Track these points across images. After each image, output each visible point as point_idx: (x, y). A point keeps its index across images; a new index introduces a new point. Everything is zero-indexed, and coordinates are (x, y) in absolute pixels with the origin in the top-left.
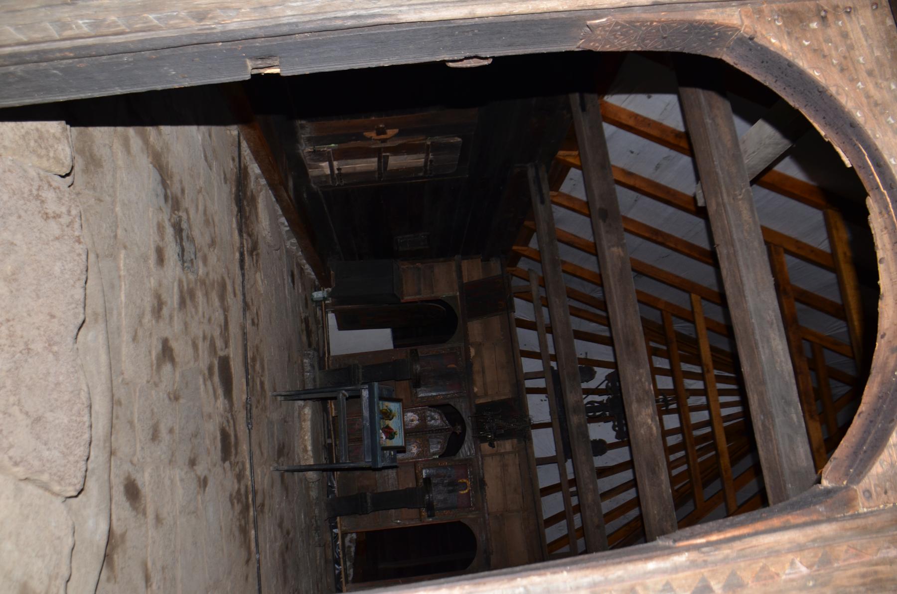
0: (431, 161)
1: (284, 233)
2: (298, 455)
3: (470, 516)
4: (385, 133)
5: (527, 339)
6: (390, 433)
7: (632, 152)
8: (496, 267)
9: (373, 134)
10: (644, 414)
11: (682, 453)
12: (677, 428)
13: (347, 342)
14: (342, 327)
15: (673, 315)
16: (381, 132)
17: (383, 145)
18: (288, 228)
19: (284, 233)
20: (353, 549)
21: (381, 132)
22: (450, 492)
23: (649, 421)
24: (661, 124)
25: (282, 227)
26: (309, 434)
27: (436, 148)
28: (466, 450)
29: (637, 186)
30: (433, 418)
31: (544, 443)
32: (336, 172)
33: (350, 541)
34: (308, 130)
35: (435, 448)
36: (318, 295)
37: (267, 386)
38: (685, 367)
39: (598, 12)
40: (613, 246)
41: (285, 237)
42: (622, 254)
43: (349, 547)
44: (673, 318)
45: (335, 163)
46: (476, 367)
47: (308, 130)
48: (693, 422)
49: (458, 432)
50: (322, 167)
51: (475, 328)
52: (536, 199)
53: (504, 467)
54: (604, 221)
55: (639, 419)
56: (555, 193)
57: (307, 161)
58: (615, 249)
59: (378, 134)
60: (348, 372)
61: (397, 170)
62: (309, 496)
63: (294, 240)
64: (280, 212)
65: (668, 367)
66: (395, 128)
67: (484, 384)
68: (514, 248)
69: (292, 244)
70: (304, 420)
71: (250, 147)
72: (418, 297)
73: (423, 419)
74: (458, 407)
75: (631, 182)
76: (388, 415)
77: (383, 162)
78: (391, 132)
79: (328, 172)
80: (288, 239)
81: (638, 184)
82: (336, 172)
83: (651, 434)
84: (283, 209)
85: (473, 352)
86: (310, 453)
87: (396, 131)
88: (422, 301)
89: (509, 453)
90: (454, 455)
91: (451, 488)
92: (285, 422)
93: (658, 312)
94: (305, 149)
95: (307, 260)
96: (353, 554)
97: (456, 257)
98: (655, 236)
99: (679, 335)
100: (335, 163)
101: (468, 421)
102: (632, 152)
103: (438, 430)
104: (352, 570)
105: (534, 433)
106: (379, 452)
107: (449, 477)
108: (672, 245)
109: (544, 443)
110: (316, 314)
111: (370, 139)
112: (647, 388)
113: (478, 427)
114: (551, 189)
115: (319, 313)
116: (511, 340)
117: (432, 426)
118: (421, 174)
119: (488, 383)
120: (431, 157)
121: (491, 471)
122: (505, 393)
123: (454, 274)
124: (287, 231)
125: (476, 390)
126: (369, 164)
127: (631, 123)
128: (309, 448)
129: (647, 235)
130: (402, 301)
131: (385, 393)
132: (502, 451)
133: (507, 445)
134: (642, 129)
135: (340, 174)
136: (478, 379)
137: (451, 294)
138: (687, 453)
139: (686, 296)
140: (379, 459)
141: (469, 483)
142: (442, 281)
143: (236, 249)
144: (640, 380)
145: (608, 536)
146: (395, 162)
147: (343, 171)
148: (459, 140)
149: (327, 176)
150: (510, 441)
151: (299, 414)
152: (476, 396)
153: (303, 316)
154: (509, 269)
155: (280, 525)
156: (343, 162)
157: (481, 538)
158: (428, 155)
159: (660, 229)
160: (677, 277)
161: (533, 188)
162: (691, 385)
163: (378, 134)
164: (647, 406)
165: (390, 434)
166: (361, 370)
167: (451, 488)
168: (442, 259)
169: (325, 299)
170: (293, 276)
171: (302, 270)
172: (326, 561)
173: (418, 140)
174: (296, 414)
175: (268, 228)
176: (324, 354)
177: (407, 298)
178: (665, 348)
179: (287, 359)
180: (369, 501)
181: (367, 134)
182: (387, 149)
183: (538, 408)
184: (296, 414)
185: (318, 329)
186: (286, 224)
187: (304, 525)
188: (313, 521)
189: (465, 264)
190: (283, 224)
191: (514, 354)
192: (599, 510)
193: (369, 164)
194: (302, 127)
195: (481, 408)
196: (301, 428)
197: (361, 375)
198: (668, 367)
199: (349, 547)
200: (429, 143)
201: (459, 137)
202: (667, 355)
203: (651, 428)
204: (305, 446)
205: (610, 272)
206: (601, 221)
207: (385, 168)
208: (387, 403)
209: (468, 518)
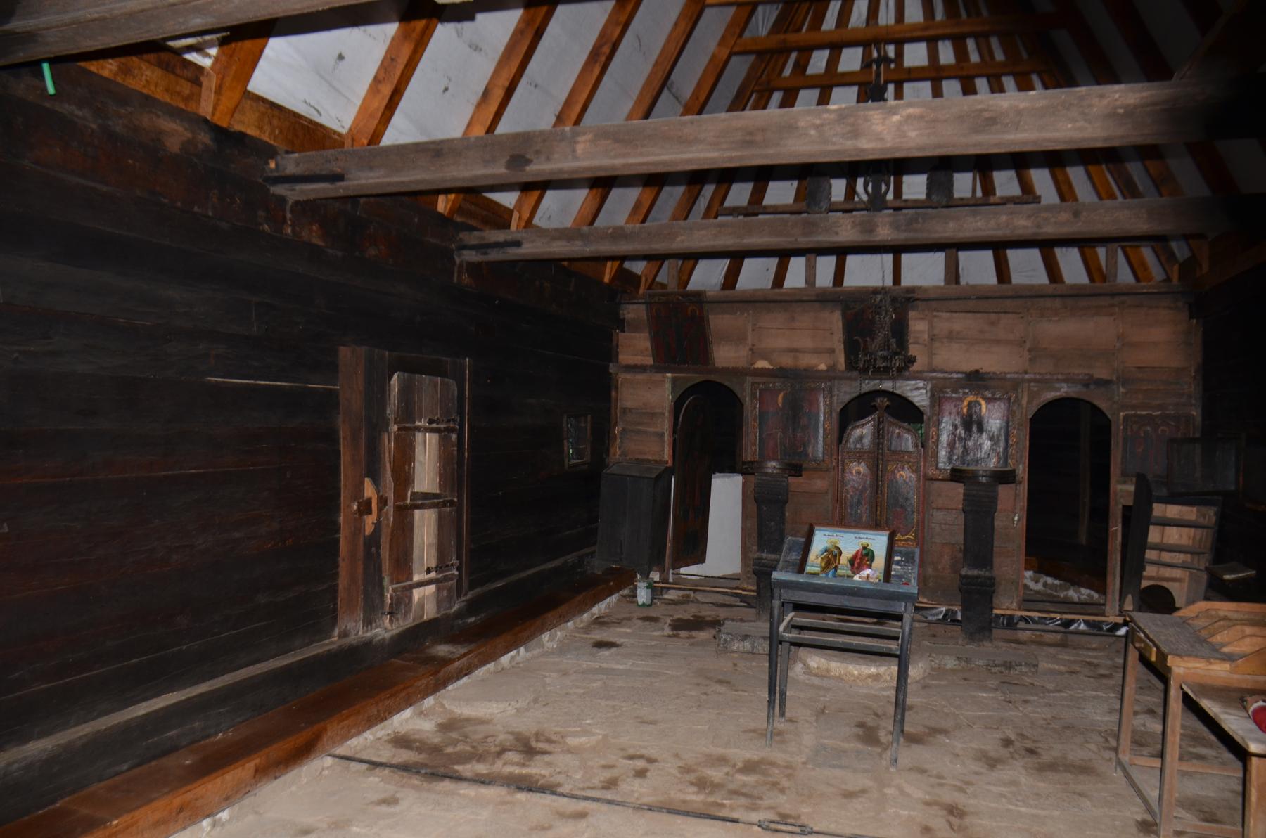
0: (431, 421)
1: (529, 655)
2: (883, 689)
3: (1024, 401)
4: (369, 502)
5: (756, 275)
6: (864, 556)
7: (446, 89)
8: (634, 311)
9: (370, 521)
10: (880, 128)
11: (971, 44)
12: (922, 69)
13: (724, 548)
14: (700, 558)
15: (741, 35)
16: (366, 508)
17: (391, 503)
18: (522, 649)
19: (529, 655)
20: (1050, 580)
21: (366, 508)
22: (981, 430)
23: (896, 118)
24: (393, 39)
25: (518, 659)
26: (850, 667)
27: (407, 413)
28: (918, 394)
29: (507, 84)
30: (861, 437)
31: (924, 271)
32: (433, 575)
33: (1037, 582)
34: (351, 625)
35: (907, 441)
36: (643, 595)
37: (752, 754)
38: (830, 22)
39: (629, 7)
40: (574, 151)
41: (537, 651)
42: (589, 137)
43: (1045, 585)
44: (747, 34)
45: (416, 578)
46: (787, 361)
47: (351, 625)
48: (921, 20)
49: (886, 402)
50: (422, 600)
51: (725, 355)
52: (513, 253)
53: (952, 337)
54: (529, 162)
55: (888, 137)
56: (516, 216)
57: (408, 622)
58: (580, 148)
59: (369, 512)
60: (759, 587)
61: (441, 476)
62: (953, 671)
63: (546, 637)
64: (491, 666)
65: (826, 53)
66: (362, 483)
67: (816, 351)
68: (607, 279)
69: (551, 639)
70: (828, 671)
71: (358, 733)
72: (666, 438)
73: (859, 456)
74: (847, 398)
75: (499, 94)
76: (832, 557)
77: (425, 500)
78: (369, 490)
79: (432, 588)
80: (543, 646)
81: (504, 82)
82: (433, 575)
83: (921, 117)
84: (484, 662)
85: (762, 364)
86: (882, 670)
87: (368, 482)
88: (674, 432)
89: (931, 326)
90: (922, 414)
91: (975, 429)
92: (823, 711)
93: (734, 59)
94: (385, 629)
95: (584, 612)
96: (1057, 582)
97: (612, 368)
98: (602, 55)
99: (778, 27)
100: (416, 578)
101: (868, 386)
102: (446, 89)
103: (879, 434)
104: (1083, 590)
105: (906, 281)
106: (890, 588)
107: (956, 427)
108: (618, 30)
109: (924, 271)
110: (674, 602)
111: (378, 525)
112: (833, 116)
113: (884, 373)
114: (506, 226)
115: (672, 595)
116: (755, 302)
117: (872, 442)
118: (454, 436)
119: (816, 344)
120: (422, 423)
121: (958, 359)
122: (835, 320)
123: (640, 377)
124: (527, 650)
125: (823, 367)
126: (425, 525)
127: (387, 90)
128: (873, 670)
129: (597, 71)
130: (670, 464)
131: (795, 557)
132: (926, 336)
133: (918, 326)
134: (398, 73)
135: (438, 569)
136: (806, 361)
137: (668, 386)
138: (971, 35)
139: (708, 13)
140: (903, 589)
141: (971, 398)
142: (647, 400)
143: (509, 798)
144: (817, 127)
145: (1101, 198)
146: (426, 477)
147: (433, 564)
148: (395, 376)
149: (438, 589)
150: (911, 323)
151: (816, 675)
152: (832, 368)
153: (668, 631)
154: (641, 291)
155: (992, 763)
156: (415, 566)
157: (1064, 390)
158: (418, 429)
159: (590, 48)
160: (676, 24)
161: (495, 256)
162: (860, 14)
163: (369, 512)
164: (866, 119)
165: (864, 558)
166: (764, 555)
167: (975, 429)
168: (613, 394)
169: (650, 586)
170: (600, 645)
171: (599, 622)
172: (1063, 645)
173: (388, 446)
174: (816, 681)
175: (502, 706)
176: (737, 595)
177: (667, 455)
178: (794, 55)
179: (722, 689)
180: (975, 572)
181: (369, 529)
182: (400, 495)
183: (867, 272)
184: (816, 681)
185: (696, 601)
186: (513, 653)
187: (999, 695)
188: (994, 670)
189: (625, 358)
190: (512, 658)
191: (776, 300)
192: (1050, 208)
193: (425, 525)
194: (344, 634)
195: (851, 365)
196: (839, 678)
197: (773, 556)
198: (826, 53)
199: (1045, 585)
200: (395, 428)
201: (391, 377)
202: (806, 51)
203: (909, 117)
204: (870, 676)
205: (618, 162)
206: (528, 168)
207: (435, 496)
208: (812, 556)
209: (1028, 406)
